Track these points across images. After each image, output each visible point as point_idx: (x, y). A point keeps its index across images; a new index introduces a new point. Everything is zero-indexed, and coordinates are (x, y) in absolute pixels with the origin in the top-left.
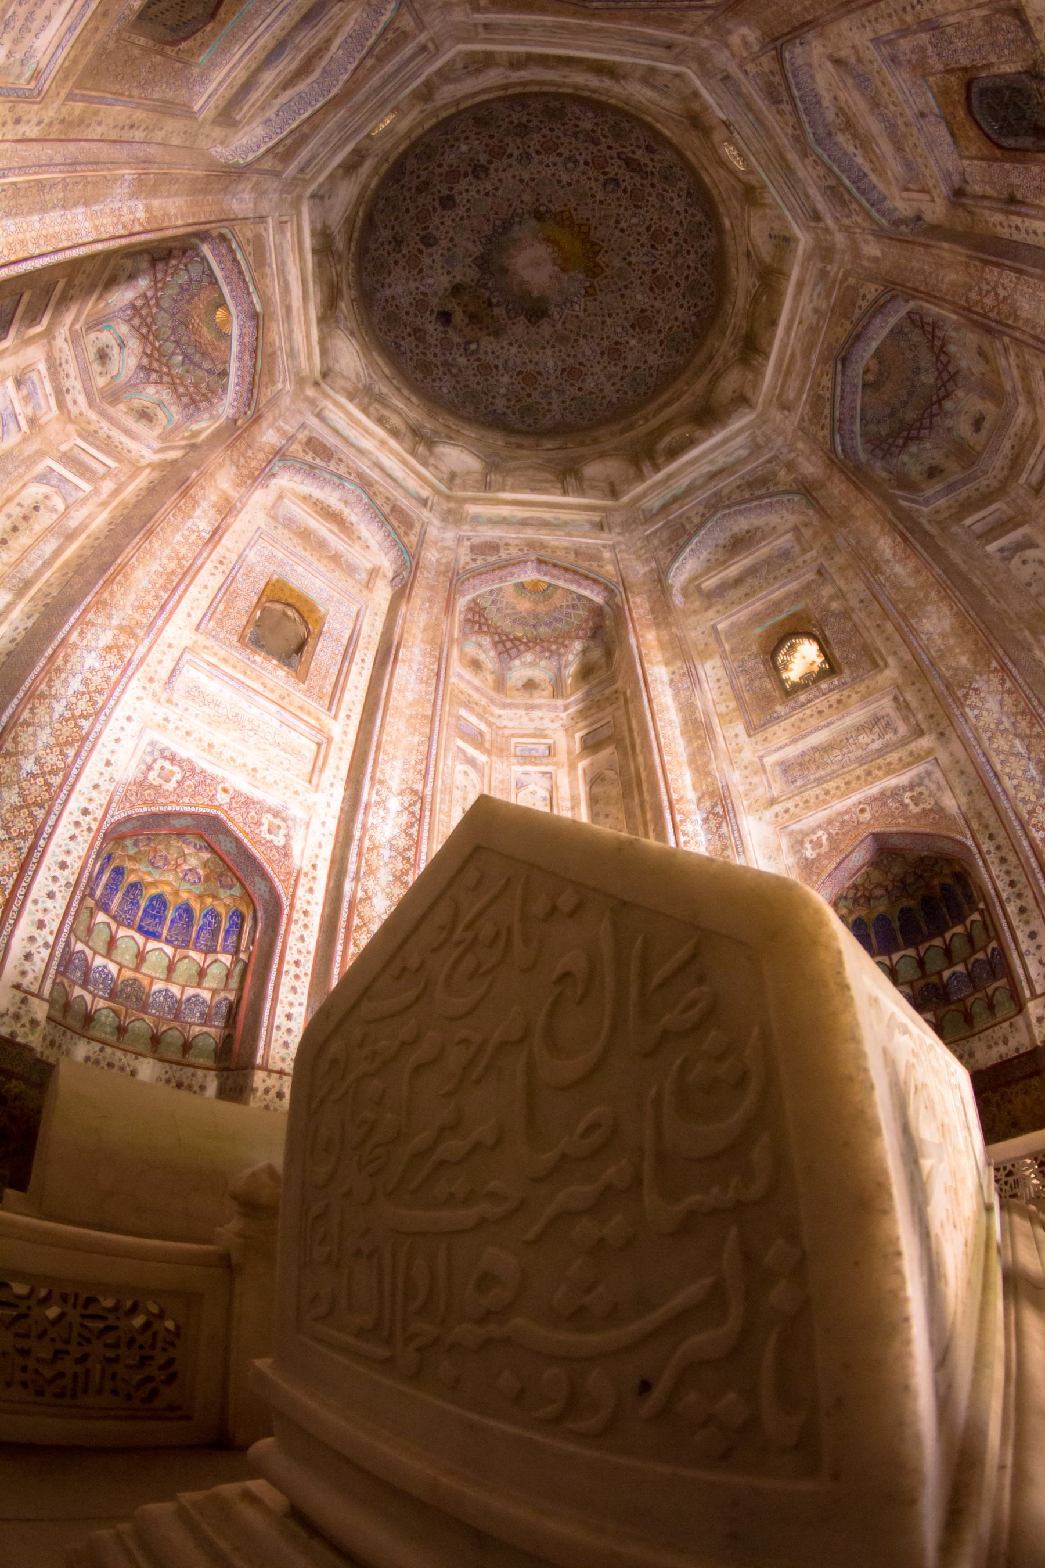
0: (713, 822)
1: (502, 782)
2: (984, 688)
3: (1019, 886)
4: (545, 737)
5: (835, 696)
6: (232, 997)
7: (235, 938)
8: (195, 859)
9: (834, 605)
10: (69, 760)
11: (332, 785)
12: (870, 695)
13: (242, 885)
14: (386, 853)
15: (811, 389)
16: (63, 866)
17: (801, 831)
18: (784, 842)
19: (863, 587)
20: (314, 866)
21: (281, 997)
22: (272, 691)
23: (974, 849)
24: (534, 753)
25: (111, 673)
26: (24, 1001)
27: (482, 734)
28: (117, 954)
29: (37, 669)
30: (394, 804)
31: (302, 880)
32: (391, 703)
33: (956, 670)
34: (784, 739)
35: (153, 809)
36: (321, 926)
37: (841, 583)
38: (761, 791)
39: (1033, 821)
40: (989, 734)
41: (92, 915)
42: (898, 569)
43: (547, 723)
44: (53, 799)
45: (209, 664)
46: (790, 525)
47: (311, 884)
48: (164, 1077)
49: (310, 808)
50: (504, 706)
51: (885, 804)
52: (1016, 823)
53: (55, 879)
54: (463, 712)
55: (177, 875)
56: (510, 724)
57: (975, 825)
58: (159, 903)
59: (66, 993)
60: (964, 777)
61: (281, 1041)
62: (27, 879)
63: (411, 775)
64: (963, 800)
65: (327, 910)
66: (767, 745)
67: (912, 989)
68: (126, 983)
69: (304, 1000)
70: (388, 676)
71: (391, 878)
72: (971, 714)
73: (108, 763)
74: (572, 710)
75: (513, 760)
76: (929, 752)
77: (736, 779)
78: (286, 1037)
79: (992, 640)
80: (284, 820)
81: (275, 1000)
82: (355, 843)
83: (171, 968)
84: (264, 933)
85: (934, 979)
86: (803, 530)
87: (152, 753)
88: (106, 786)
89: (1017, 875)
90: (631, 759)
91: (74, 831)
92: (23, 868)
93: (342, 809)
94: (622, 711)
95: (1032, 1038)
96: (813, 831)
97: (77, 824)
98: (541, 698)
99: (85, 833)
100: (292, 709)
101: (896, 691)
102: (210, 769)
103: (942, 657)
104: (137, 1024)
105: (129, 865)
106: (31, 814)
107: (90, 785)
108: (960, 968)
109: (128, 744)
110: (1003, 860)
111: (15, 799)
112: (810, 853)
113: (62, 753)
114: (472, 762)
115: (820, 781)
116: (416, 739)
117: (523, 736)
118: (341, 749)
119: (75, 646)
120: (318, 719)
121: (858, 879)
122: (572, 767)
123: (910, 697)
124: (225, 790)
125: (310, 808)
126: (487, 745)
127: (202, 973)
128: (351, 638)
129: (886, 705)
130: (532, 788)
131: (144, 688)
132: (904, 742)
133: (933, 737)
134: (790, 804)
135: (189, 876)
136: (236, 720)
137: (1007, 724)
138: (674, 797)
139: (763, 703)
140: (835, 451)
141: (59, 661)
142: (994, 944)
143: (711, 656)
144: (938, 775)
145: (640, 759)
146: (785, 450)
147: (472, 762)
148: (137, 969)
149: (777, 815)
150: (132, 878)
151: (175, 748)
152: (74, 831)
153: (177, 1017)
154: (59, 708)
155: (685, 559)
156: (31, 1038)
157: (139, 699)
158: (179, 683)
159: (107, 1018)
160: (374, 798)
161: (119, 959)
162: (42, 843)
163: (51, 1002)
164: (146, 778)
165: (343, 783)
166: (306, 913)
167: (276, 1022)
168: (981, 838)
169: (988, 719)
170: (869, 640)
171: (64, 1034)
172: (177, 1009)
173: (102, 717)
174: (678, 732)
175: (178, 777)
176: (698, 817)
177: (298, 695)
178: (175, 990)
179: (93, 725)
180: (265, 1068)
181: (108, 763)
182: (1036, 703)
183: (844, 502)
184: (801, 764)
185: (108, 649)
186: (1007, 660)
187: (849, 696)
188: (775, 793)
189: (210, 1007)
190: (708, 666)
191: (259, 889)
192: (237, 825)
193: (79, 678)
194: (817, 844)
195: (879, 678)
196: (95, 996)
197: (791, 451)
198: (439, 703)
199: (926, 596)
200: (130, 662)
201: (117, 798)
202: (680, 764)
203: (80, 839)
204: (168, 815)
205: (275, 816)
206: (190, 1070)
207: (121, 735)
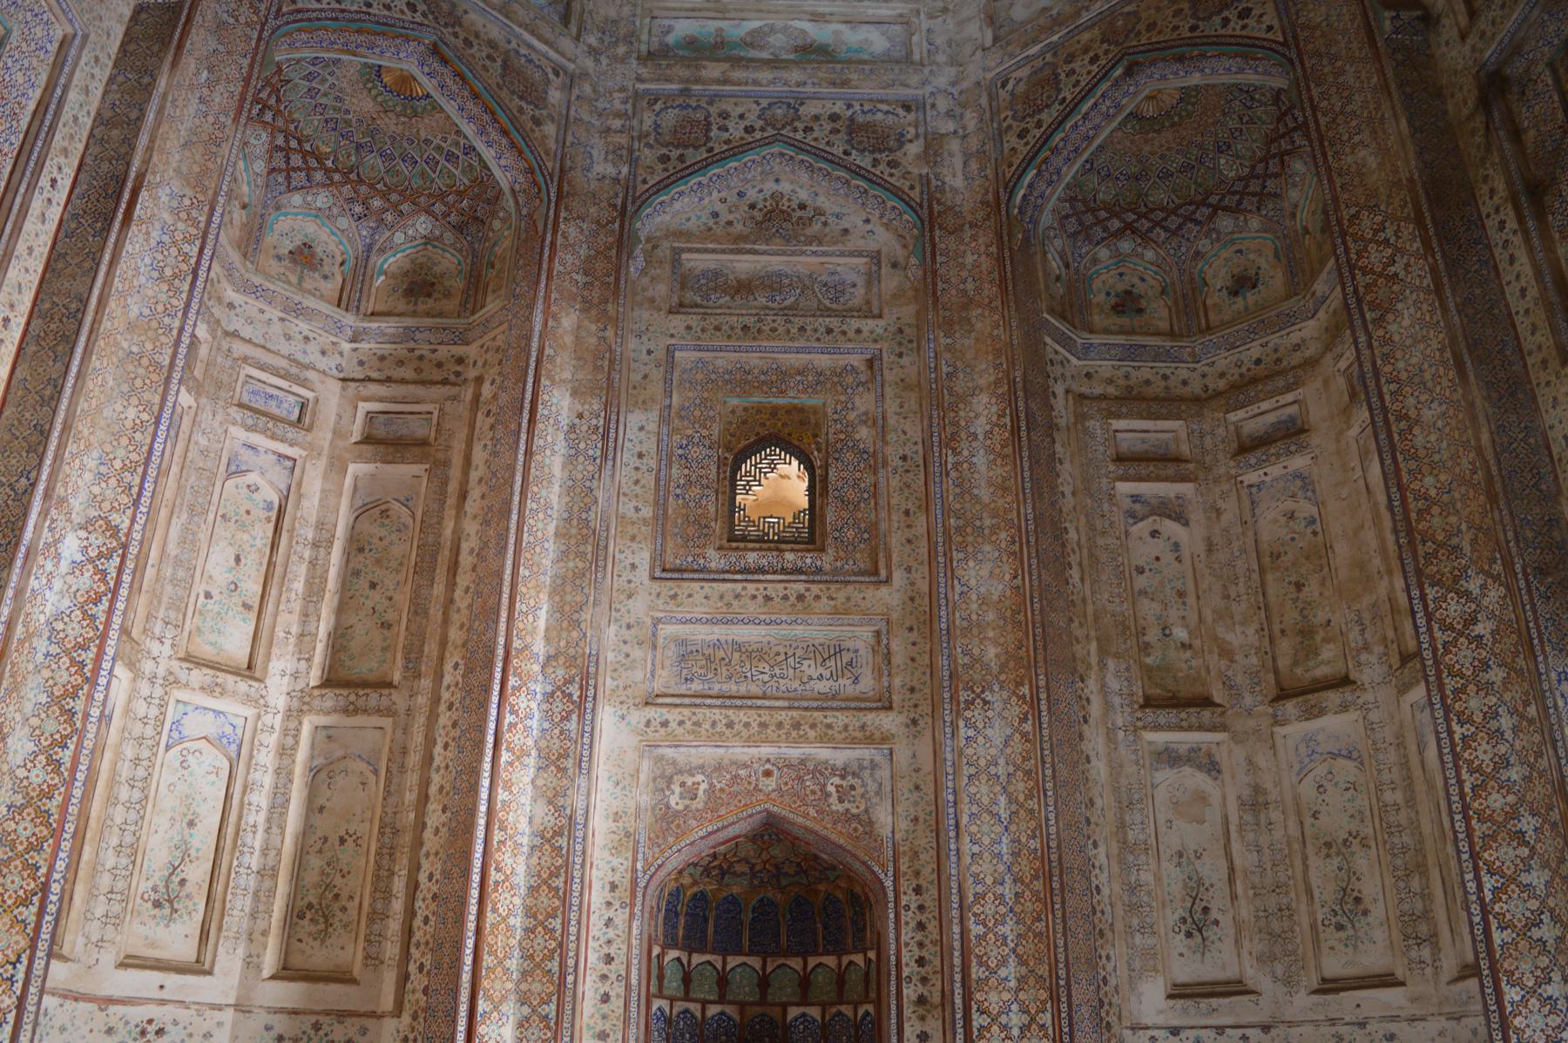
0: (558, 706)
2: (998, 706)
4: (304, 383)
9: (863, 433)
15: (1054, 49)
16: (609, 959)
19: (918, 437)
23: (891, 895)
37: (891, 406)
38: (639, 675)
40: (972, 771)
42: (980, 460)
46: (873, 246)
51: (800, 779)
52: (955, 898)
60: (915, 795)
63: (110, 490)
64: (903, 825)
66: (672, 606)
67: (742, 1013)
79: (1040, 658)
85: (775, 1012)
86: (885, 270)
90: (450, 513)
101: (882, 626)
103: (966, 631)
108: (814, 1012)
110: (921, 926)
116: (131, 413)
122: (337, 466)
123: (899, 647)
128: (42, 106)
129: (860, 637)
130: (253, 478)
132: (859, 704)
133: (902, 719)
134: (673, 716)
138: (517, 644)
139: (691, 531)
140: (1011, 194)
143: (645, 405)
144: (884, 773)
146: (943, 104)
149: (648, 724)
155: (681, 194)
168: (905, 885)
169: (981, 751)
170: (883, 526)
174: (551, 529)
182: (1049, 772)
183: (970, 286)
184: (708, 658)
186: (1043, 696)
187: (817, 597)
195: (870, 593)
197: (950, 114)
199: (994, 529)
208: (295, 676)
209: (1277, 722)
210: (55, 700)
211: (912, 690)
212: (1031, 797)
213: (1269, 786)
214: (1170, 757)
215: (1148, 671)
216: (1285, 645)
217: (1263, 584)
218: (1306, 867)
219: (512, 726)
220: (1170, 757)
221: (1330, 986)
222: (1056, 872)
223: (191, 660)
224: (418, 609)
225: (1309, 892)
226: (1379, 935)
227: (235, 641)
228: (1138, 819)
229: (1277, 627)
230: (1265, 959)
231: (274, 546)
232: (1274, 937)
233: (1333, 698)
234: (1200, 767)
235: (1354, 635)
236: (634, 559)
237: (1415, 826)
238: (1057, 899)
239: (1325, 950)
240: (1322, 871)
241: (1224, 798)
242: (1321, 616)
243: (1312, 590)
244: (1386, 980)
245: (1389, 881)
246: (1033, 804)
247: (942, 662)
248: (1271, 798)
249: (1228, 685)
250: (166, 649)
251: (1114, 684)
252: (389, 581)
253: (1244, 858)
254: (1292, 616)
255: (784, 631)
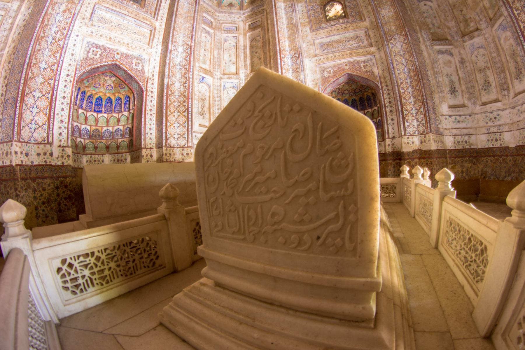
0: (294, 59)
1: (219, 40)
2: (398, 39)
3: (392, 104)
4: (235, 24)
5: (344, 25)
6: (130, 126)
7: (128, 106)
8: (110, 81)
10: (58, 59)
11: (157, 45)
12: (357, 28)
13: (128, 87)
14: (178, 67)
16: (64, 98)
17: (324, 67)
18: (318, 70)
20: (153, 75)
21: (147, 123)
22: (132, 13)
23: (380, 88)
24: (231, 29)
25: (67, 20)
26: (63, 150)
27: (212, 23)
28: (89, 122)
29: (38, 28)
30: (180, 49)
31: (149, 81)
32: (178, 13)
33: (390, 30)
34: (323, 35)
35: (92, 67)
36: (157, 96)
38: (312, 51)
39: (401, 86)
41: (77, 111)
43: (236, 19)
44: (55, 75)
45: (106, 7)
47: (152, 81)
48: (113, 159)
49: (150, 54)
50: (220, 12)
51: (354, 65)
52: (396, 84)
53: (62, 103)
54: (205, 15)
55: (105, 88)
56: (222, 19)
57: (382, 80)
58: (100, 99)
59: (75, 142)
60: (382, 65)
61: (149, 138)
62: (53, 107)
64: (381, 71)
65: (159, 90)
66: (316, 36)
68: (93, 131)
69: (154, 122)
70: (176, 3)
71: (181, 76)
72: (390, 46)
73: (73, 55)
74: (246, 15)
75: (223, 32)
76: (373, 53)
77: (304, 45)
78: (150, 136)
80: (141, 60)
81: (145, 124)
82: (167, 65)
83: (108, 121)
84: (138, 102)
87: (88, 46)
88: (74, 63)
89: (392, 100)
90: (267, 34)
91: (65, 84)
92: (51, 104)
93: (161, 53)
94: (265, 17)
95: (385, 150)
96: (328, 68)
97: (66, 81)
98: (235, 10)
99: (69, 83)
100: (140, 19)
102: (111, 47)
103: (386, 24)
104: (100, 144)
105: (86, 89)
106: (48, 83)
107: (67, 65)
109: (79, 45)
110: (389, 94)
111: (42, 80)
112: (326, 75)
113: (54, 56)
114: (208, 33)
115: (333, 52)
116: (188, 26)
117: (227, 23)
118: (159, 32)
119: (51, 14)
120: (150, 21)
121: (341, 86)
122: (245, 35)
123: (371, 33)
124: (118, 54)
125: (150, 54)
126: (213, 26)
127: (118, 120)
129: (362, 33)
130: (229, 42)
131: (81, 23)
132: (365, 47)
133: (375, 48)
134: (322, 58)
135: (109, 88)
136: (119, 27)
137: (402, 53)
138: (282, 49)
139: (317, 22)
141: (46, 22)
142: (380, 118)
144: (374, 61)
145: (270, 34)
147: (208, 33)
148: (96, 125)
150: (89, 94)
151: (97, 42)
152: (65, 84)
153: (113, 138)
154: (50, 40)
156: (69, 162)
157: (80, 27)
158: (95, 18)
159: (90, 145)
160: (173, 48)
161: (89, 124)
162: (55, 92)
163: (72, 147)
164: (88, 56)
165: (161, 44)
166: (152, 92)
167: (146, 132)
169: (396, 50)
170: (361, 10)
171: (78, 156)
172: (112, 135)
173: (67, 38)
174: (285, 27)
175: (100, 53)
176: (289, 57)
177: (142, 14)
178: (110, 129)
179: (64, 42)
180: (145, 148)
181: (73, 55)
185: (65, 11)
186: (408, 33)
188: (317, 53)
189: (123, 131)
190: (300, 5)
191: (134, 86)
192: (124, 65)
193: (55, 26)
194: (329, 73)
195: (361, 24)
196: (84, 139)
198: (196, 12)
200: (74, 14)
201: (78, 67)
202: (285, 38)
203: (68, 86)
204: (98, 67)
205: (137, 60)
206: (120, 155)
207: (76, 43)
208: (245, 73)
209: (464, 42)
210: (183, 76)
211: (377, 42)
212: (410, 57)
213: (465, 57)
214: (441, 52)
215: (432, 34)
216: (462, 25)
217: (453, 12)
218: (476, 77)
219: (284, 65)
220: (441, 52)
221: (484, 104)
222: (420, 74)
223: (224, 74)
224: (265, 53)
225: (477, 82)
226: (494, 90)
227: (233, 69)
228: (436, 66)
229: (459, 21)
230: (469, 99)
231: (236, 52)
232: (471, 93)
233: (476, 33)
234: (448, 54)
235: (477, 18)
236: (305, 30)
237: (501, 61)
238: (421, 80)
239: (482, 96)
240: (480, 77)
241: (455, 61)
242: (468, 16)
243: (465, 11)
244: (497, 101)
245: (496, 76)
246: (411, 59)
247: (382, 32)
248: (466, 60)
249: (451, 35)
250: (219, 73)
251: (425, 36)
252: (259, 51)
253: (461, 75)
254: (461, 18)
255: (343, 36)
